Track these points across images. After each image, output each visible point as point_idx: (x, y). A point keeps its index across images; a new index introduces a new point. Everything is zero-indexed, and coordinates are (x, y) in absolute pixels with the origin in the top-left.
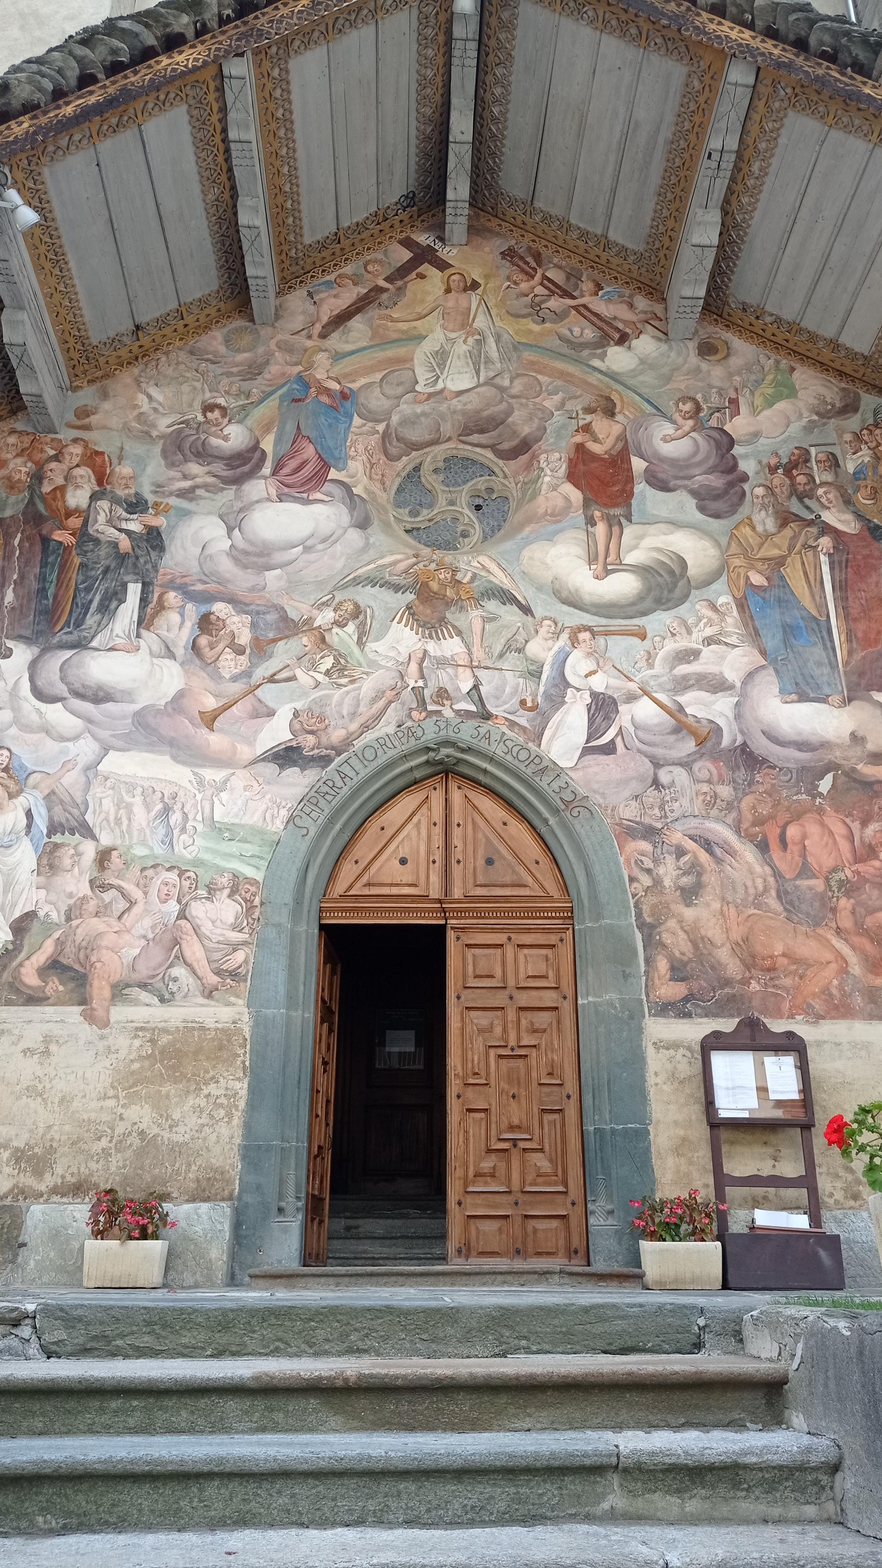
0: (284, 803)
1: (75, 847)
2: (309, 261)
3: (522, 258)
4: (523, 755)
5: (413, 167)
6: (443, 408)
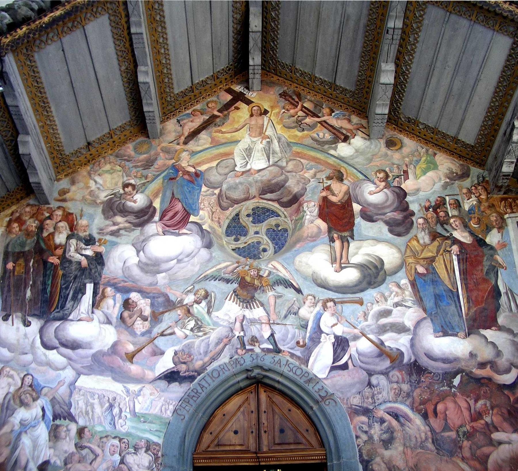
0: (171, 402)
1: (67, 427)
2: (177, 102)
3: (291, 97)
4: (299, 372)
5: (231, 48)
6: (251, 179)
